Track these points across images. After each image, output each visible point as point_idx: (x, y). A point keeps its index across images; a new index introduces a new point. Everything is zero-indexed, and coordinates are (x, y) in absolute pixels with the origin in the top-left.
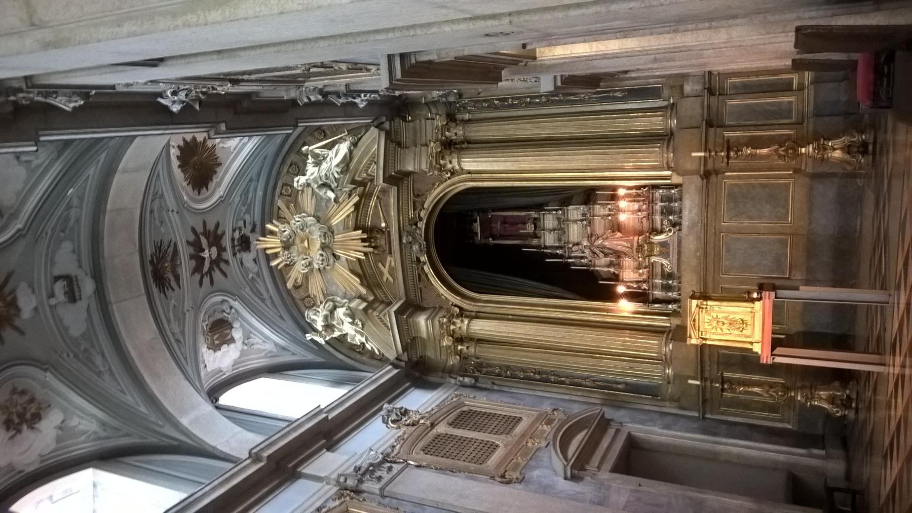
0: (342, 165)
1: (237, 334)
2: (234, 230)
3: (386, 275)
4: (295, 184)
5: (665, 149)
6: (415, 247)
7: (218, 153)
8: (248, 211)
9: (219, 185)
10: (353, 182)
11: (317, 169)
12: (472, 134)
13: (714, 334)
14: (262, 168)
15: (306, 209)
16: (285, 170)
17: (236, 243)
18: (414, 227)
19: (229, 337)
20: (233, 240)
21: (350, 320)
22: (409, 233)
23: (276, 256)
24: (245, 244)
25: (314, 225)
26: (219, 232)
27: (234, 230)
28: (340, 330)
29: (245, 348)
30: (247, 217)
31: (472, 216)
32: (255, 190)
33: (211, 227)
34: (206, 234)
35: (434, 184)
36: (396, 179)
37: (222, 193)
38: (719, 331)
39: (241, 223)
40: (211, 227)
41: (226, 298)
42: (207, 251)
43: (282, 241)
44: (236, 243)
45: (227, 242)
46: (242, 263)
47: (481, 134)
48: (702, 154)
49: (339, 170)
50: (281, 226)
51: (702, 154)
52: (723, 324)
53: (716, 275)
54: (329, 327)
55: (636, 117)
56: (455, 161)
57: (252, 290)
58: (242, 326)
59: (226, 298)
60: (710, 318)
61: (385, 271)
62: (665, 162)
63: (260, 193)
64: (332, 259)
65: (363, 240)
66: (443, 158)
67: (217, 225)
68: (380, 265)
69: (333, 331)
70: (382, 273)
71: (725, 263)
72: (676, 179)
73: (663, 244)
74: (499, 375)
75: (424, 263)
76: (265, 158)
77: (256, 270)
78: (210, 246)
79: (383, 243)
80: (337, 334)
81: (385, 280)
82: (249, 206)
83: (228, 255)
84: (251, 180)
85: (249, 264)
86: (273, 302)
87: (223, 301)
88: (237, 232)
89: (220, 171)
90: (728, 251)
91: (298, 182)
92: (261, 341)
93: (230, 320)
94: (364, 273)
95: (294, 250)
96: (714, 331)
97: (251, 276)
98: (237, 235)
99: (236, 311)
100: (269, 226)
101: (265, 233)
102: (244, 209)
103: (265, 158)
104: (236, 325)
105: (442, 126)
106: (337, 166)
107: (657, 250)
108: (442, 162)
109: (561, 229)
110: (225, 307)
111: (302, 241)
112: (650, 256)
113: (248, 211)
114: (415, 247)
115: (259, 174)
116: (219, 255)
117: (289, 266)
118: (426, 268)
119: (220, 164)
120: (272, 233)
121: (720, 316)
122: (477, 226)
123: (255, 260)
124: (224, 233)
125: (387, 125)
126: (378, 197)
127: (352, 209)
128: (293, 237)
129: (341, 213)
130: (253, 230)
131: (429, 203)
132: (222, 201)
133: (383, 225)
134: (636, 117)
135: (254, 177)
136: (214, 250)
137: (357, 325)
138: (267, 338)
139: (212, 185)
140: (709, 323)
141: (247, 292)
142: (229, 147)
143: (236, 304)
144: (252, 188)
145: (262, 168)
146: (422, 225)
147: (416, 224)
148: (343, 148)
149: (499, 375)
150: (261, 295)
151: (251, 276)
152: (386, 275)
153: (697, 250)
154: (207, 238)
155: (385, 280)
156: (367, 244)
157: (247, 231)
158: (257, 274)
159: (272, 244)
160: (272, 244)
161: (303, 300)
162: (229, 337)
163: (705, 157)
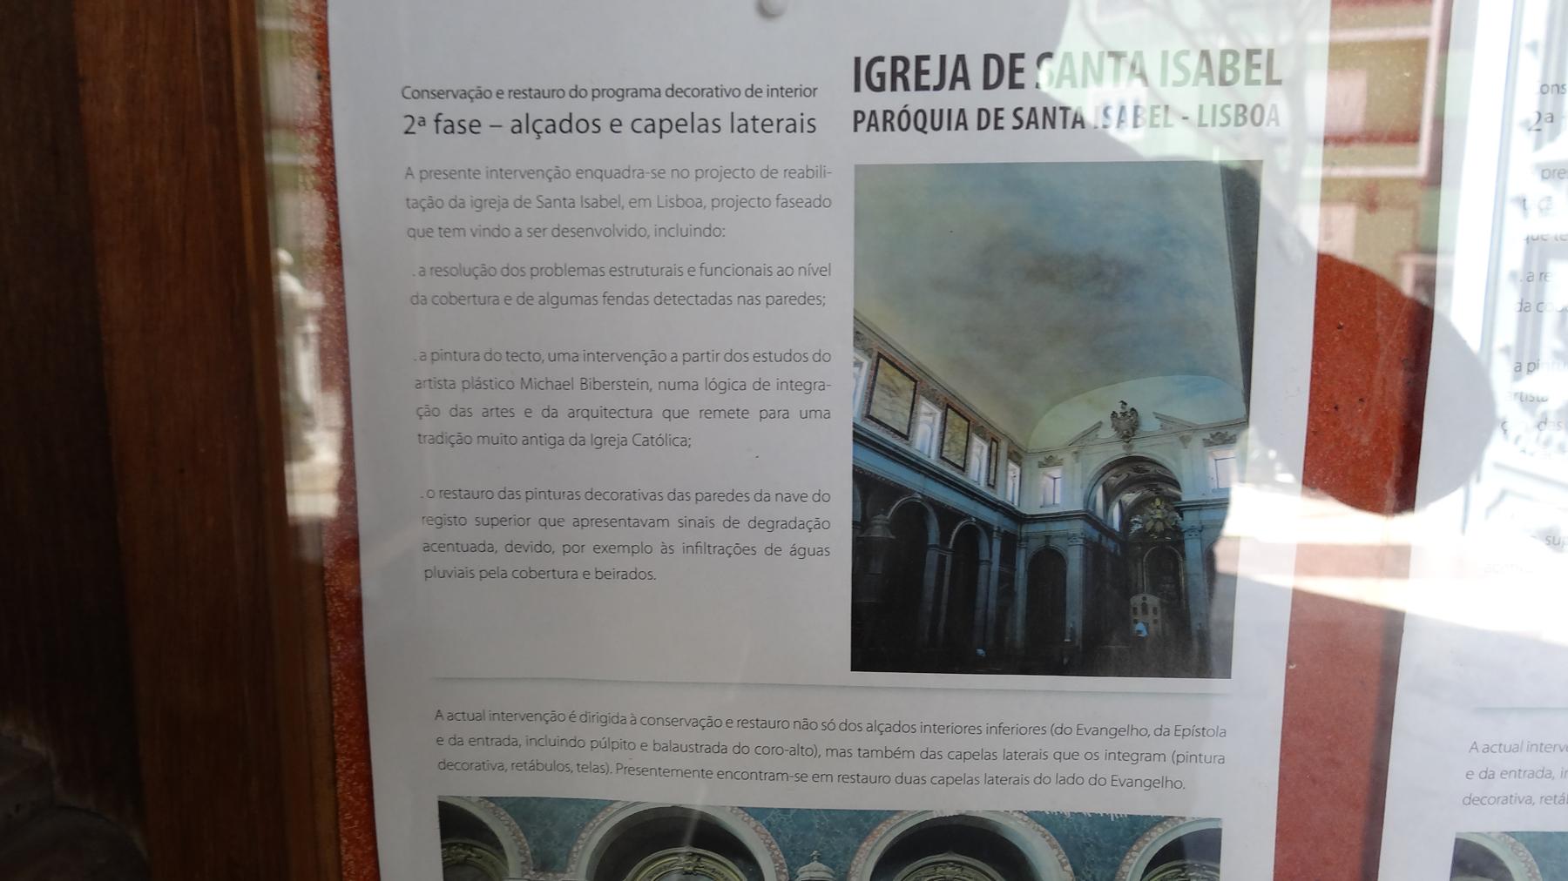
94: (1153, 530)
159: (1158, 502)
160: (1158, 502)
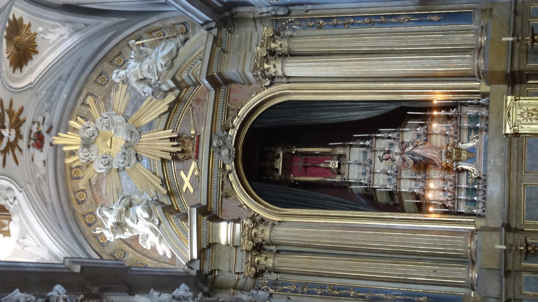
0: (167, 59)
1: (14, 227)
2: (34, 123)
3: (187, 184)
4: (114, 76)
5: (476, 55)
6: (225, 152)
7: (38, 41)
8: (48, 110)
9: (31, 71)
10: (174, 79)
11: (139, 64)
12: (297, 46)
13: (525, 124)
14: (73, 69)
15: (116, 107)
16: (94, 78)
17: (32, 135)
18: (225, 133)
19: (5, 229)
20: (31, 131)
21: (146, 215)
22: (220, 138)
23: (72, 153)
24: (38, 141)
25: (122, 124)
26: (21, 117)
27: (34, 123)
28: (131, 230)
29: (19, 247)
30: (47, 115)
31: (275, 152)
32: (61, 91)
33: (16, 108)
34: (11, 113)
35: (250, 95)
36: (219, 82)
37: (33, 80)
38: (529, 121)
39: (40, 119)
40: (16, 108)
41: (12, 186)
42: (7, 130)
43: (83, 139)
44: (32, 135)
45: (24, 130)
46: (33, 159)
47: (305, 46)
48: (511, 39)
49: (163, 63)
50: (86, 124)
51: (511, 39)
52: (533, 115)
53: (519, 175)
54: (120, 226)
55: (400, 275)
56: (279, 65)
57: (37, 189)
58: (20, 222)
59: (12, 186)
60: (522, 111)
61: (186, 180)
62: (475, 67)
63: (64, 96)
64: (134, 159)
65: (172, 139)
66: (267, 62)
67: (21, 110)
68: (182, 174)
69: (123, 231)
70: (182, 182)
71: (528, 162)
72: (485, 88)
73: (471, 151)
74: (295, 292)
75: (230, 172)
76: (78, 61)
77: (43, 171)
78: (11, 127)
79: (190, 148)
80: (127, 235)
81: (184, 189)
82: (52, 104)
83: (23, 144)
84: (60, 79)
85: (39, 163)
86: (54, 210)
87: (9, 189)
88: (36, 125)
89: (36, 59)
90: (530, 151)
91: (118, 73)
92: (35, 245)
93: (11, 211)
95: (93, 148)
96: (525, 121)
97: (38, 175)
98: (35, 129)
99: (19, 204)
100: (73, 123)
101: (67, 129)
102: (46, 105)
103: (78, 61)
104: (15, 218)
105: (268, 37)
106: (163, 58)
107: (464, 155)
108: (266, 66)
109: (368, 165)
110: (9, 195)
111: (105, 140)
112: (457, 161)
113: (48, 110)
114: (225, 152)
115: (69, 75)
116: (16, 140)
117: (89, 164)
118: (231, 177)
119: (36, 52)
120: (75, 130)
121: (530, 108)
122: (279, 164)
123: (44, 162)
124: (24, 121)
125: (215, 31)
126: (191, 105)
127: (166, 109)
128: (96, 134)
129: (153, 113)
130: (49, 131)
131: (243, 112)
132: (30, 87)
133: (193, 132)
134: (400, 275)
135: (64, 77)
136: (13, 132)
137: (153, 222)
138: (43, 243)
139: (26, 69)
140: (521, 115)
141: (31, 189)
142: (49, 40)
143: (20, 196)
144: (58, 88)
145: (73, 69)
146: (233, 133)
147: (228, 131)
148: (171, 46)
149: (295, 292)
150: (45, 198)
151: (38, 175)
152: (187, 184)
153: (502, 150)
154: (11, 118)
155: (184, 189)
156: (175, 143)
157: (44, 129)
158: (44, 176)
159: (69, 141)
160: (69, 141)
161: (84, 216)
162: (5, 229)
163: (513, 42)
